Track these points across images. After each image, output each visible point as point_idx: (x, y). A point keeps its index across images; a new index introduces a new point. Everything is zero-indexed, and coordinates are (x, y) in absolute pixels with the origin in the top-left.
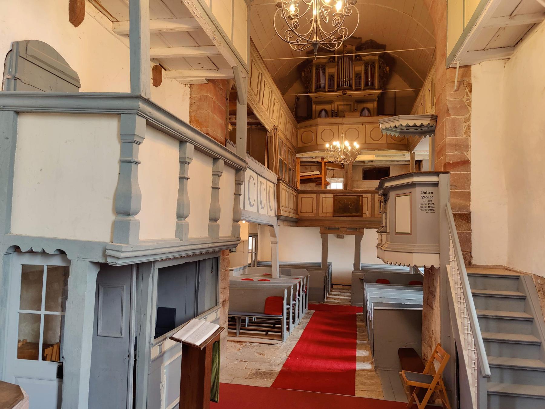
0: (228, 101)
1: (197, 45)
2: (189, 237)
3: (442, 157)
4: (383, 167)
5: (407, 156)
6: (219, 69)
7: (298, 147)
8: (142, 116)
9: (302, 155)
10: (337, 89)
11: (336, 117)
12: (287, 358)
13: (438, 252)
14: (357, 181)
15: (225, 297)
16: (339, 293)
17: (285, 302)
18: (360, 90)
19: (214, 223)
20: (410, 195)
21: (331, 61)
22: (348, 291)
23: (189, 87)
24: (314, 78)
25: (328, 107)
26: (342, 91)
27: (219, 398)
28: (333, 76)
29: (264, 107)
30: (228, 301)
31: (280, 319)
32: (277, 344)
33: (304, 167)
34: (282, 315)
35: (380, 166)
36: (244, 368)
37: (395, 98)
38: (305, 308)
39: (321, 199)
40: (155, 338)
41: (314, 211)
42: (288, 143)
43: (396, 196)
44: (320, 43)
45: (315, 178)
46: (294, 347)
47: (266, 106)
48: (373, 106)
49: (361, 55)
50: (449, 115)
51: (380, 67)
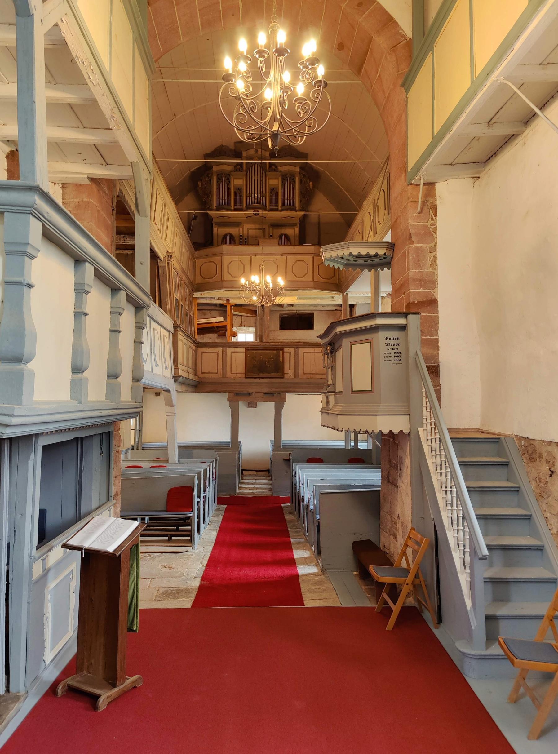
0: (115, 212)
1: (81, 126)
2: (88, 400)
3: (404, 295)
4: (306, 313)
5: (338, 299)
6: (107, 164)
7: (196, 283)
8: (37, 217)
9: (201, 294)
10: (246, 207)
11: (245, 244)
12: (204, 568)
13: (407, 413)
14: (274, 331)
15: (116, 490)
16: (253, 481)
17: (195, 493)
18: (276, 210)
19: (113, 381)
20: (371, 342)
21: (238, 170)
22: (264, 478)
23: (61, 188)
24: (215, 190)
25: (234, 231)
26: (253, 210)
27: (138, 625)
28: (240, 190)
29: (156, 224)
30: (120, 495)
31: (189, 518)
32: (187, 551)
33: (201, 312)
34: (192, 511)
35: (302, 311)
36: (147, 588)
37: (319, 223)
38: (214, 503)
39: (229, 354)
40: (37, 548)
41: (220, 371)
42: (184, 277)
43: (352, 343)
44: (282, 134)
45: (218, 327)
46: (209, 553)
47: (158, 224)
48: (293, 232)
49: (276, 164)
50: (412, 243)
51: (301, 181)
